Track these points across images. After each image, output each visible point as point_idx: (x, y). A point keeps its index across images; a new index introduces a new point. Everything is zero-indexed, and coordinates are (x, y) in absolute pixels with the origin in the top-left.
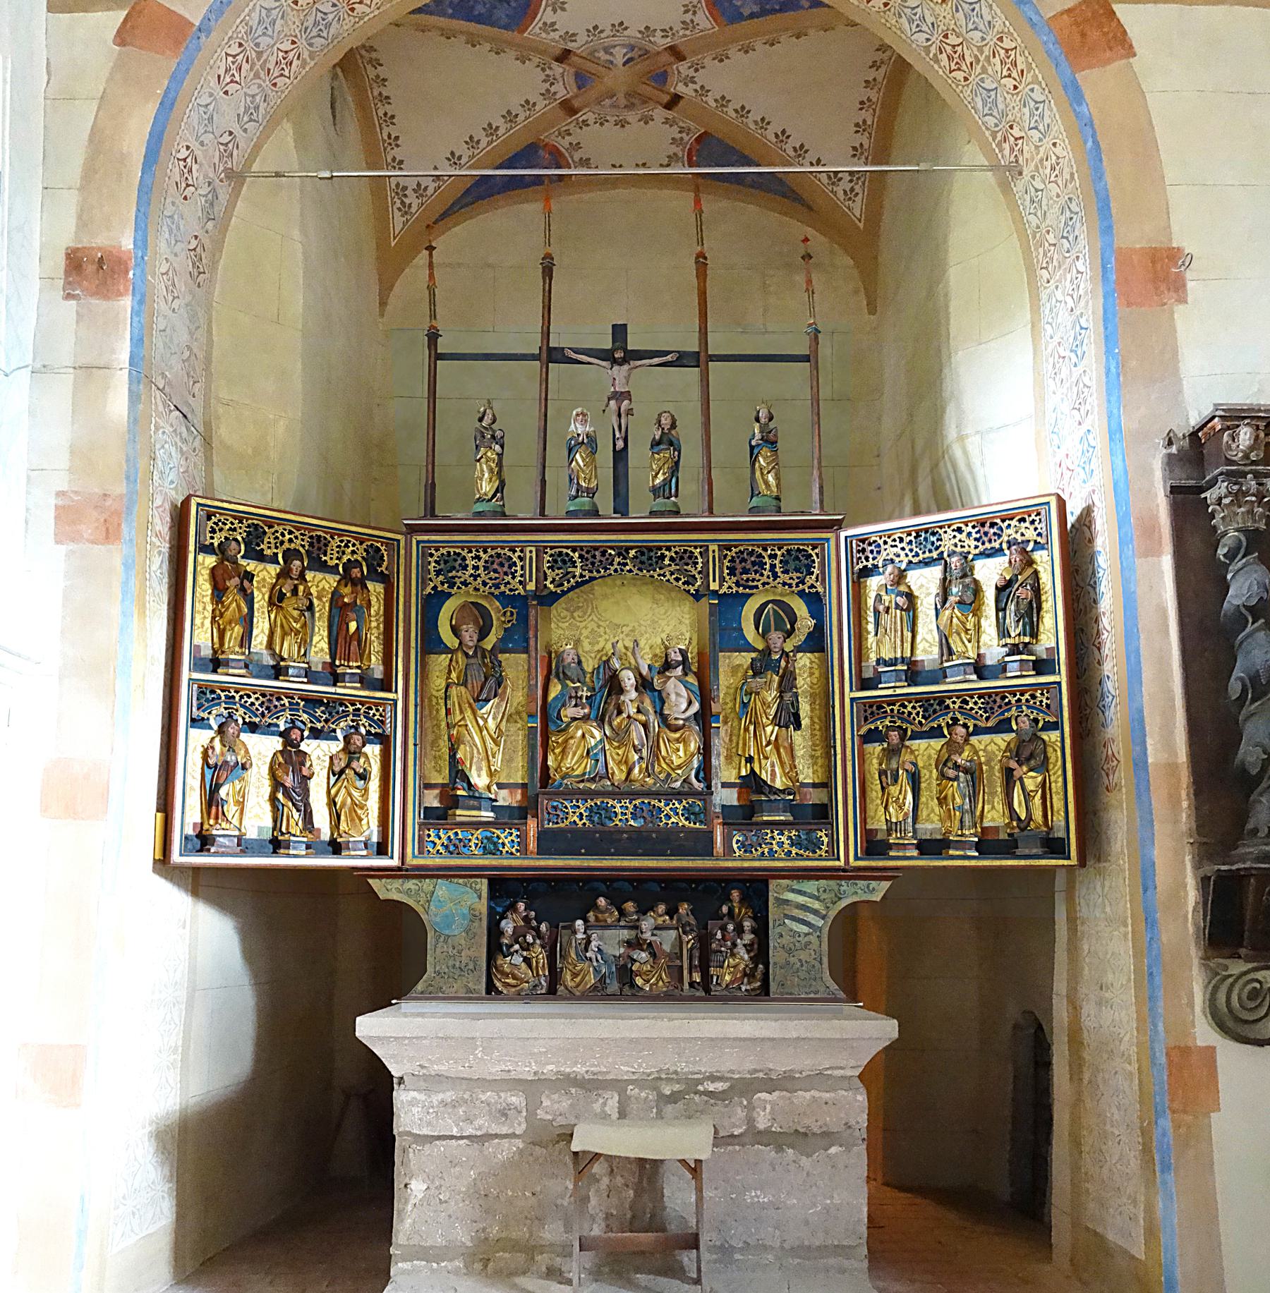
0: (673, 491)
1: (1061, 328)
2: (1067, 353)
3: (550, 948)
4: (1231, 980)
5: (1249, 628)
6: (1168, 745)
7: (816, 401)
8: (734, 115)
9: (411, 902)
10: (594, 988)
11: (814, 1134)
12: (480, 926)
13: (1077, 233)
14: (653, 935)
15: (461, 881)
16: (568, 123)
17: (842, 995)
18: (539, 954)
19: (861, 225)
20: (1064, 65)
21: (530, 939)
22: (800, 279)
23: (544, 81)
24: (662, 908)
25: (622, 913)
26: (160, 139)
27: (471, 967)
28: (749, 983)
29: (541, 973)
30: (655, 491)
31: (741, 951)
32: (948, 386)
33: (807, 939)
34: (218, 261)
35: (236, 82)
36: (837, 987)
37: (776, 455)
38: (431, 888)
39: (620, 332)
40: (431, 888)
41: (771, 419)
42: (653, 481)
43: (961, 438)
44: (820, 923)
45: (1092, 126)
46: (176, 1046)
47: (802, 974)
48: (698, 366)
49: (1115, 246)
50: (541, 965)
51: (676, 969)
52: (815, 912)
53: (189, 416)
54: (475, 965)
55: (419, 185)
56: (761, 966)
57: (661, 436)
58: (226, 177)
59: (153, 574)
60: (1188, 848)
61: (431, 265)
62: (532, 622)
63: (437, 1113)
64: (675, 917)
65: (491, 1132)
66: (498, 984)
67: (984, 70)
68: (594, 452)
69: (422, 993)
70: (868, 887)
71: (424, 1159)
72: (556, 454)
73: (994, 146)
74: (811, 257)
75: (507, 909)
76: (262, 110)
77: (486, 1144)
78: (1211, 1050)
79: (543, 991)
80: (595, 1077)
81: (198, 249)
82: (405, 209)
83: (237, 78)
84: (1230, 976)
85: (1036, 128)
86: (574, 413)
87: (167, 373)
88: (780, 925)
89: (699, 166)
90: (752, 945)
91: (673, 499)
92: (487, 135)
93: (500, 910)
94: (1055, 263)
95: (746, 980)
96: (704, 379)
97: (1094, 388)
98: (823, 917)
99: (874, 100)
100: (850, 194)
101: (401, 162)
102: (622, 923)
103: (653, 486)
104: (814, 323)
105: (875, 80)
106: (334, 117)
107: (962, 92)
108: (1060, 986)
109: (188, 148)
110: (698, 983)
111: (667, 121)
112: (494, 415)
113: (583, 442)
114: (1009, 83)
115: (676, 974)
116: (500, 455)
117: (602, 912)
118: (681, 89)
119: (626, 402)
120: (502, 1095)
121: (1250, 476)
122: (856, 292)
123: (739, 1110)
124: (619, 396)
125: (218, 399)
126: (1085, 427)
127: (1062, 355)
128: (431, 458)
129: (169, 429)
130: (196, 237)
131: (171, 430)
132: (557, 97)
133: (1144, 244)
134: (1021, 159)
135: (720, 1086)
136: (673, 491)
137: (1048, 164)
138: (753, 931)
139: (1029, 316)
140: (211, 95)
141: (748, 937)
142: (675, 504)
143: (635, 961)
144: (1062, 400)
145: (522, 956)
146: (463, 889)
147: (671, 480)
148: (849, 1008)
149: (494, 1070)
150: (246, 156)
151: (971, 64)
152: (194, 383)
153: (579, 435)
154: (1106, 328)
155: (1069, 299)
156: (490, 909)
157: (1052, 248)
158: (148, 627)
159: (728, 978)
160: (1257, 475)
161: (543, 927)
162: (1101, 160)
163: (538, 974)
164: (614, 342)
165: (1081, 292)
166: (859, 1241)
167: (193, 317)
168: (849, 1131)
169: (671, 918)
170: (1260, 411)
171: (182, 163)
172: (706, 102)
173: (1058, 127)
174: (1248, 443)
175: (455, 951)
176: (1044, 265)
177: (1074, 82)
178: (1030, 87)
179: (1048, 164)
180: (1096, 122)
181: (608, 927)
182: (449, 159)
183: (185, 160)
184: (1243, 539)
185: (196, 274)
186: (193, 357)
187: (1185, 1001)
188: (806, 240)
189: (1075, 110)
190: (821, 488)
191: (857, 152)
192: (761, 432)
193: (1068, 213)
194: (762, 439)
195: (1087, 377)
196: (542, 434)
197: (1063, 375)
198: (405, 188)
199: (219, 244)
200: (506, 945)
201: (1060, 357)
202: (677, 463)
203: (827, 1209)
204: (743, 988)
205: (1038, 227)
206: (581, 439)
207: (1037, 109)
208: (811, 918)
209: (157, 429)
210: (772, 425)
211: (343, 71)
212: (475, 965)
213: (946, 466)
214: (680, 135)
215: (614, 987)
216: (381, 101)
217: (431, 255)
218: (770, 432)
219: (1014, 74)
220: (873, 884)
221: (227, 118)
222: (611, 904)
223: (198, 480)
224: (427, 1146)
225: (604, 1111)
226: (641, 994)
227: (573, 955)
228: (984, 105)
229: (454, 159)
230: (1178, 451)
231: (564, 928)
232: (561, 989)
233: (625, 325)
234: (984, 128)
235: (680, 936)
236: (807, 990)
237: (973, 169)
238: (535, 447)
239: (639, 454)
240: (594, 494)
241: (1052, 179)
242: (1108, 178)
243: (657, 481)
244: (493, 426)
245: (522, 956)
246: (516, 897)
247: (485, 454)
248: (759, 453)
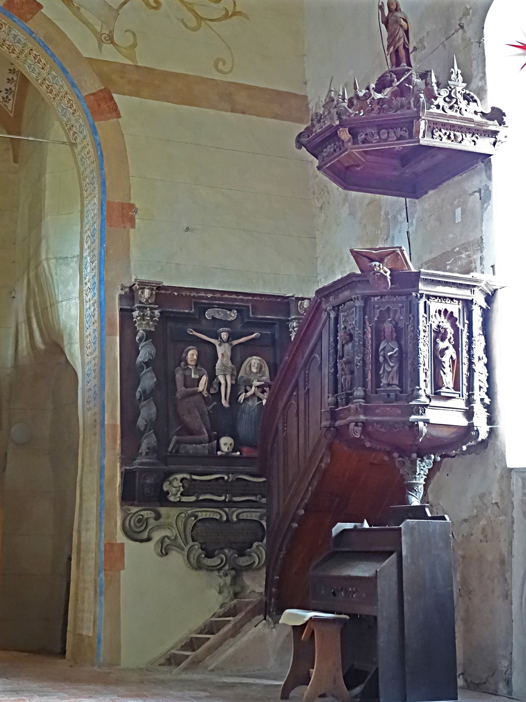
4: (131, 515)
5: (145, 371)
6: (114, 417)
19: (12, 115)
20: (91, 118)
45: (100, 146)
49: (107, 200)
60: (118, 460)
62: (258, 510)
78: (122, 545)
84: (131, 513)
121: (148, 309)
122: (7, 149)
133: (119, 201)
160: (151, 309)
162: (103, 161)
170: (153, 283)
174: (147, 296)
180: (102, 145)
184: (145, 334)
187: (113, 524)
230: (125, 293)
242: (106, 170)
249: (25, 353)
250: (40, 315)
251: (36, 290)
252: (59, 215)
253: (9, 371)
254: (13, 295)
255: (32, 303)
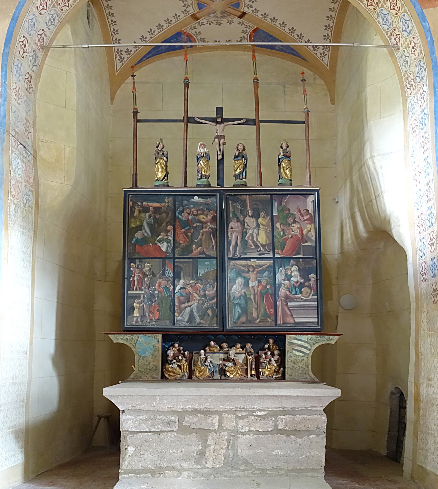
0: (244, 176)
1: (416, 114)
2: (419, 124)
3: (189, 361)
7: (308, 140)
8: (270, 21)
9: (128, 344)
10: (209, 377)
11: (303, 431)
12: (158, 353)
13: (423, 75)
14: (234, 356)
15: (150, 335)
16: (194, 23)
17: (317, 380)
18: (185, 364)
19: (328, 68)
20: (418, 6)
21: (180, 358)
22: (300, 89)
23: (184, 6)
24: (239, 346)
25: (221, 348)
26: (12, 33)
27: (154, 368)
28: (277, 375)
29: (185, 371)
30: (236, 176)
31: (274, 363)
32: (366, 136)
33: (302, 358)
34: (39, 83)
35: (45, 9)
36: (314, 377)
37: (291, 163)
38: (137, 338)
39: (219, 110)
40: (137, 338)
41: (288, 147)
42: (235, 172)
43: (372, 157)
44: (308, 352)
45: (430, 32)
46: (23, 399)
47: (300, 372)
48: (255, 125)
50: (185, 368)
51: (245, 370)
52: (306, 348)
53: (26, 147)
54: (156, 367)
55: (127, 49)
56: (282, 368)
57: (239, 154)
58: (41, 48)
59: (11, 212)
61: (134, 83)
63: (139, 423)
64: (244, 349)
65: (163, 430)
66: (166, 375)
67: (382, 6)
68: (208, 160)
69: (133, 379)
70: (329, 338)
71: (133, 440)
72: (192, 161)
73: (387, 37)
74: (305, 80)
75: (170, 346)
76: (56, 21)
77: (161, 434)
79: (186, 378)
80: (209, 410)
81: (29, 78)
82: (122, 59)
83: (45, 8)
85: (406, 31)
86: (199, 144)
87: (16, 130)
88: (290, 353)
89: (254, 42)
90: (278, 360)
91: (244, 180)
92: (158, 29)
93: (167, 346)
94: (414, 87)
95: (275, 374)
96: (258, 130)
97: (430, 139)
98: (309, 350)
99: (333, 16)
100: (323, 55)
101: (119, 40)
102: (221, 351)
103: (235, 174)
104: (307, 108)
105: (334, 8)
106: (89, 23)
107: (373, 14)
108: (411, 378)
109: (24, 37)
110: (254, 375)
111: (240, 23)
112: (163, 145)
113: (203, 156)
114: (394, 12)
115: (245, 371)
116: (166, 162)
117: (212, 347)
118: (246, 10)
119: (223, 140)
120: (168, 416)
122: (326, 95)
123: (271, 422)
124: (219, 137)
125: (39, 139)
126: (426, 155)
127: (416, 124)
128: (135, 163)
129: (17, 152)
130: (28, 73)
131: (19, 152)
132: (189, 13)
134: (399, 43)
135: (263, 413)
136: (244, 176)
137: (411, 46)
138: (279, 355)
139: (402, 107)
140: (34, 15)
141: (276, 357)
142: (245, 182)
143: (227, 366)
144: (416, 143)
145: (177, 364)
146: (150, 338)
147: (243, 172)
148: (320, 384)
149: (164, 407)
150: (50, 40)
151: (377, 3)
152: (28, 133)
153: (201, 153)
154: (435, 115)
155: (419, 102)
156: (163, 346)
157: (412, 81)
158: (9, 234)
159: (267, 373)
161: (186, 353)
163: (184, 371)
164: (217, 115)
165: (425, 99)
166: (321, 467)
167: (28, 106)
168: (318, 430)
169: (243, 350)
171: (21, 43)
172: (258, 16)
173: (415, 31)
175: (147, 363)
176: (409, 87)
177: (422, 13)
178: (403, 14)
179: (411, 46)
181: (215, 353)
182: (141, 39)
183: (23, 42)
185: (29, 88)
186: (28, 122)
188: (303, 73)
189: (422, 25)
190: (310, 176)
191: (325, 37)
192: (283, 152)
193: (419, 66)
194: (284, 155)
195: (427, 134)
196: (185, 153)
197: (417, 133)
198: (121, 51)
199: (38, 76)
200: (170, 360)
201: (415, 125)
202: (246, 165)
203: (308, 457)
204: (274, 377)
205: (406, 72)
206: (202, 155)
207: (406, 23)
208: (304, 350)
209: (12, 152)
210: (288, 150)
211: (92, 3)
212: (156, 367)
213: (365, 169)
214: (246, 29)
215: (217, 376)
216: (110, 15)
217: (134, 79)
218: (287, 153)
219: (396, 8)
220: (332, 337)
221: (41, 24)
222: (216, 344)
223: (31, 174)
224: (135, 435)
225: (212, 422)
226: (229, 379)
227: (199, 364)
228: (383, 20)
229: (143, 39)
231: (195, 353)
232: (194, 377)
233: (222, 107)
234: (383, 30)
235: (246, 357)
236: (302, 378)
237: (378, 46)
238: (182, 158)
239: (228, 161)
240: (208, 178)
241: (413, 52)
243: (237, 173)
244: (163, 150)
245: (177, 364)
246: (174, 341)
247: (160, 161)
248: (282, 161)
249: (350, 242)
250: (365, 208)
251: (360, 188)
252: (381, 118)
253: (336, 257)
254: (336, 201)
255: (355, 201)
